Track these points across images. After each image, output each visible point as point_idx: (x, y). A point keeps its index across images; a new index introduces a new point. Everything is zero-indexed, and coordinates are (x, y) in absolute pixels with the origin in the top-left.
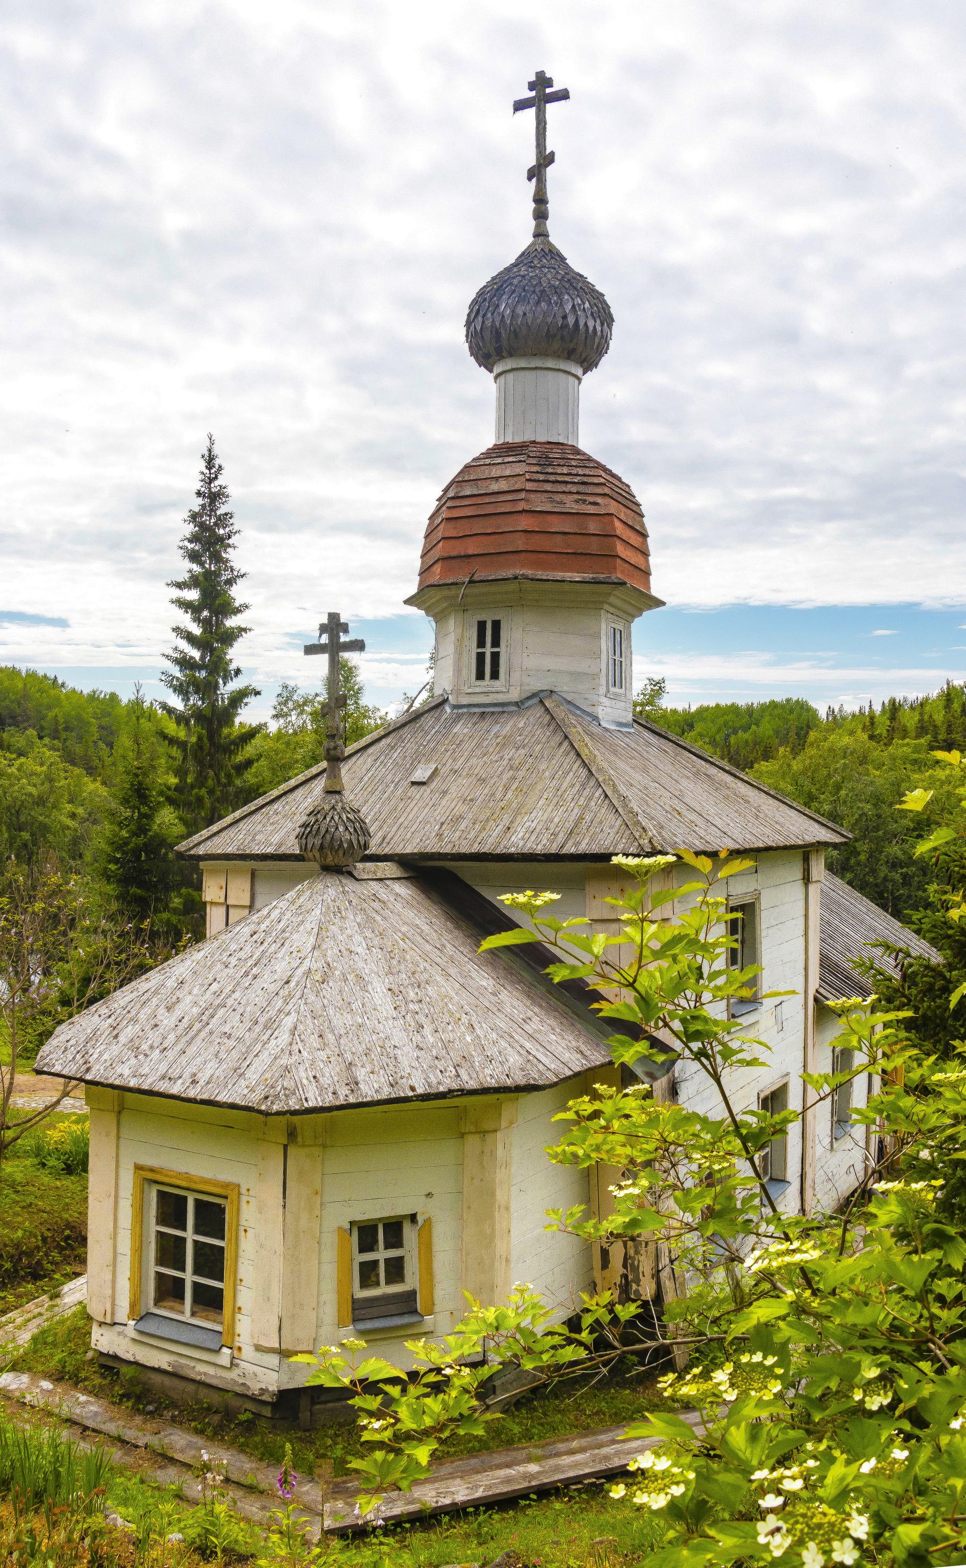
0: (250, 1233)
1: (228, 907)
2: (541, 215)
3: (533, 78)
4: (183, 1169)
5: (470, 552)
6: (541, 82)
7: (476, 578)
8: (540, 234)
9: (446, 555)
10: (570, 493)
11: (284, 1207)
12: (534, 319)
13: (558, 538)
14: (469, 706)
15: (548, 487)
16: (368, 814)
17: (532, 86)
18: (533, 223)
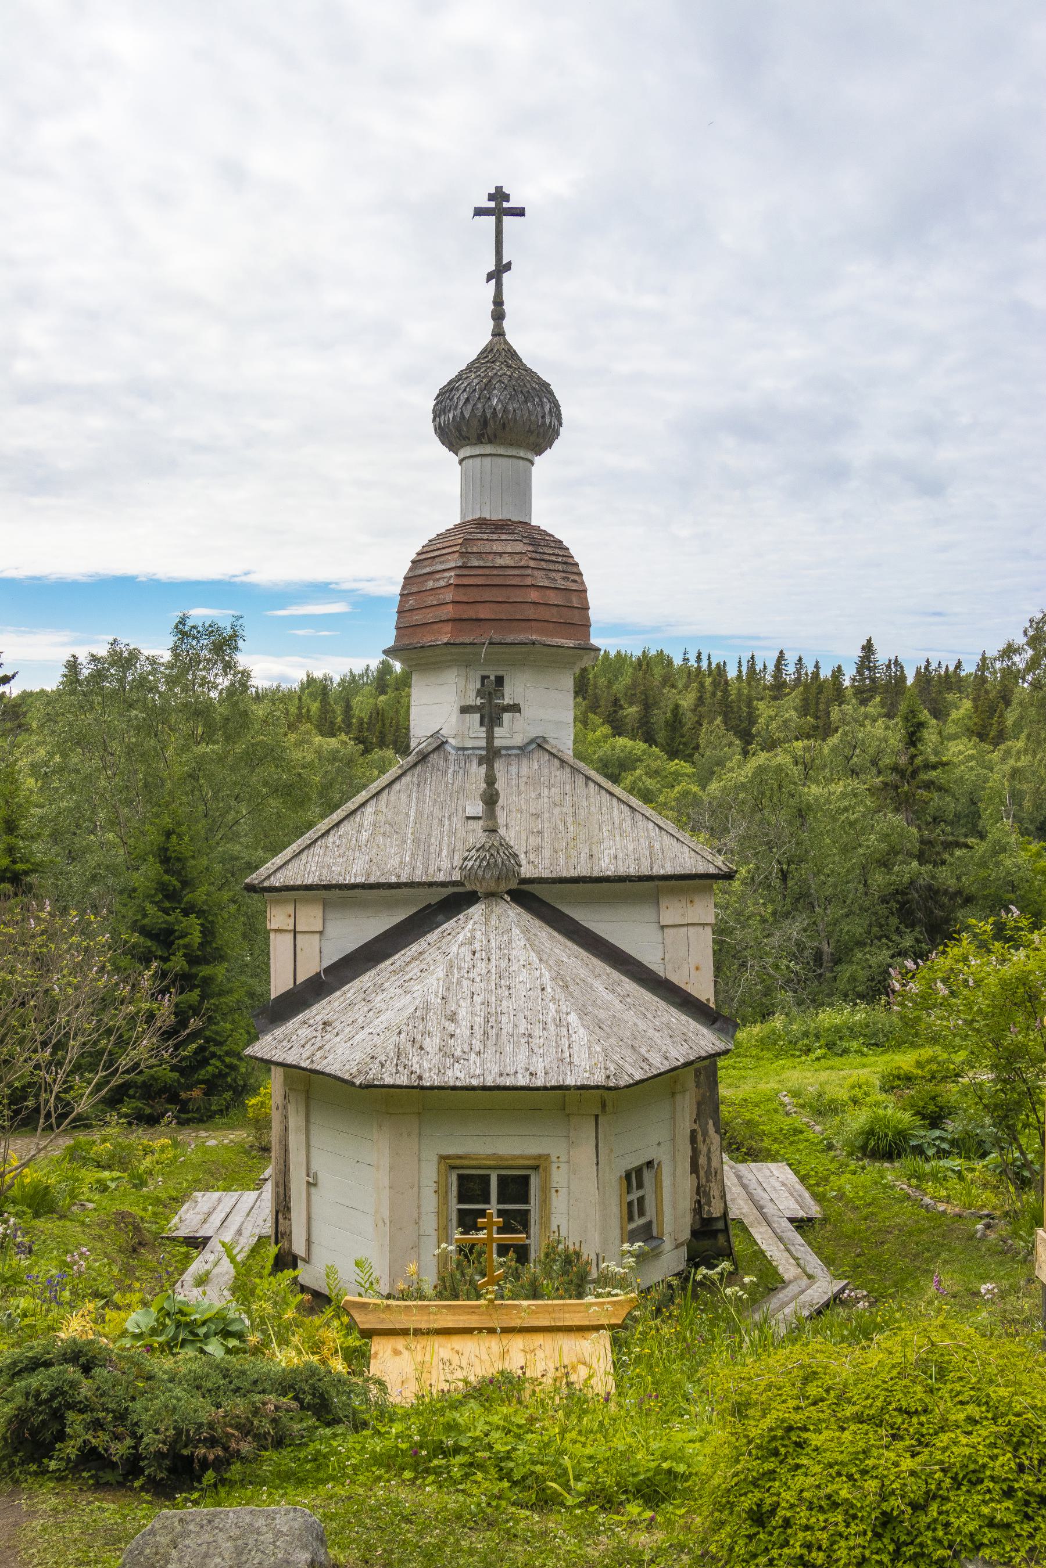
0: (563, 1192)
1: (295, 932)
2: (498, 315)
3: (493, 191)
4: (491, 1151)
5: (482, 616)
6: (499, 195)
7: (494, 641)
8: (498, 333)
9: (458, 617)
10: (558, 571)
11: (597, 1164)
12: (522, 416)
13: (554, 610)
14: (473, 748)
15: (544, 565)
16: (519, 848)
17: (491, 197)
18: (492, 323)
